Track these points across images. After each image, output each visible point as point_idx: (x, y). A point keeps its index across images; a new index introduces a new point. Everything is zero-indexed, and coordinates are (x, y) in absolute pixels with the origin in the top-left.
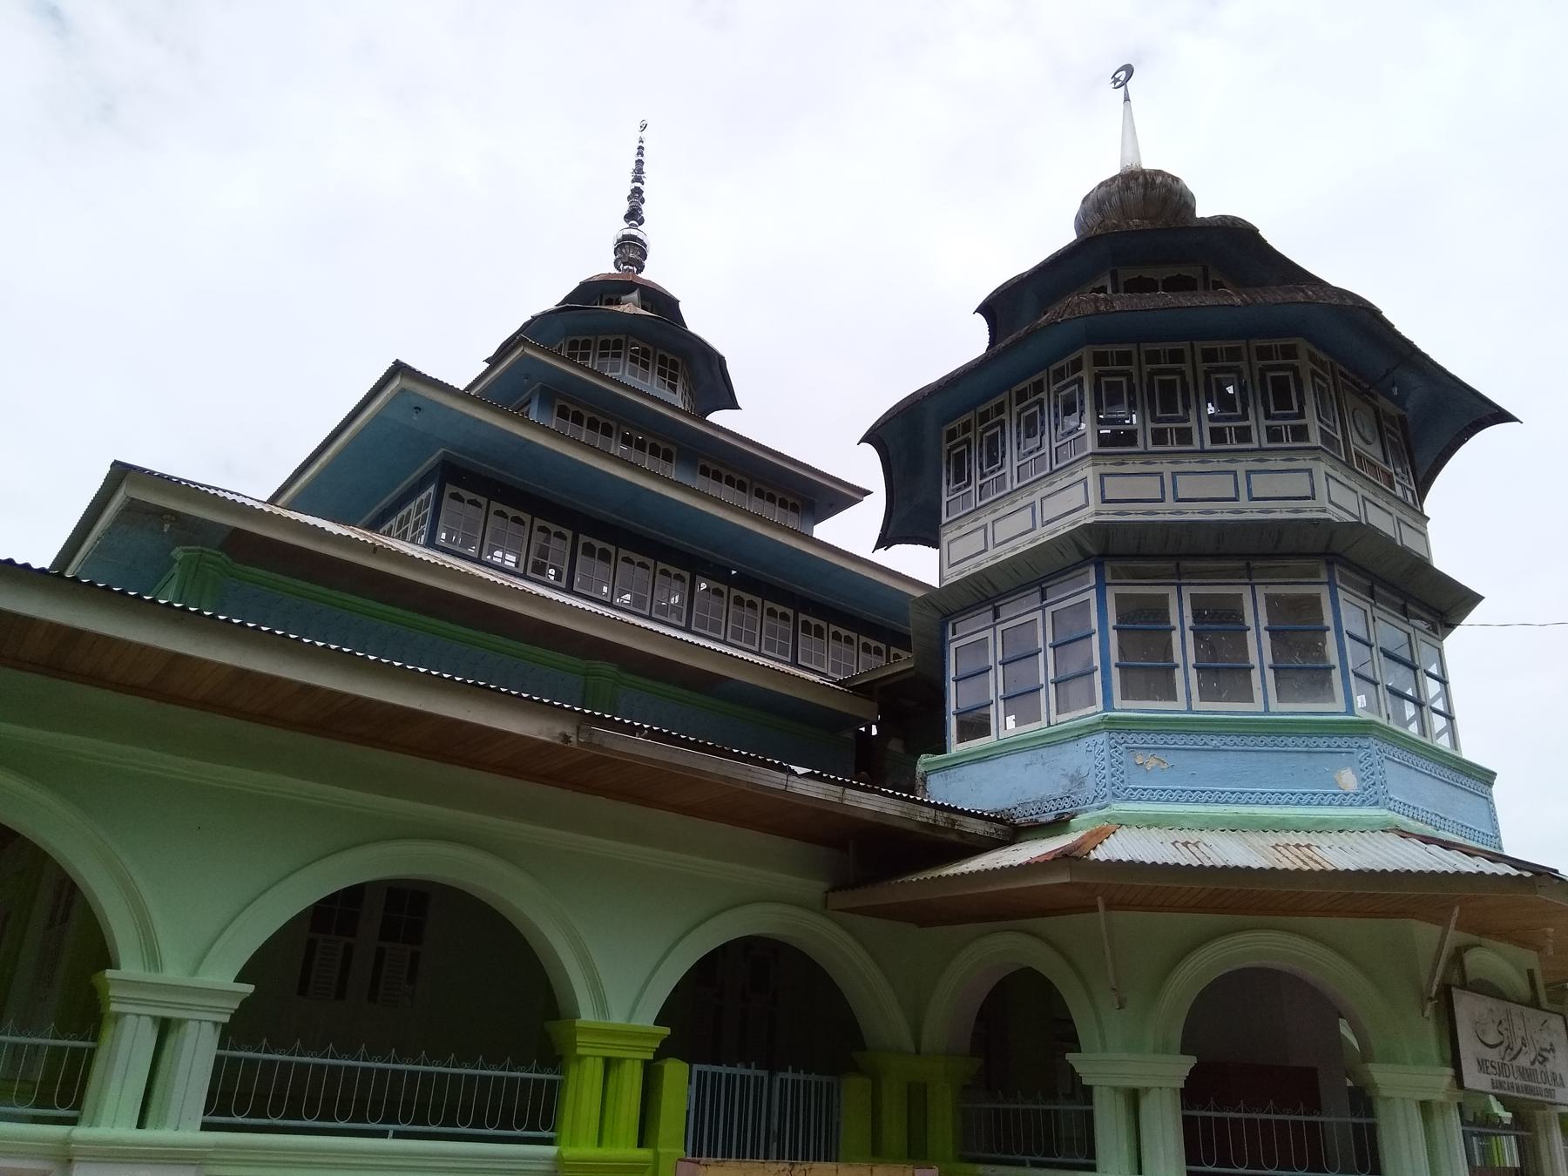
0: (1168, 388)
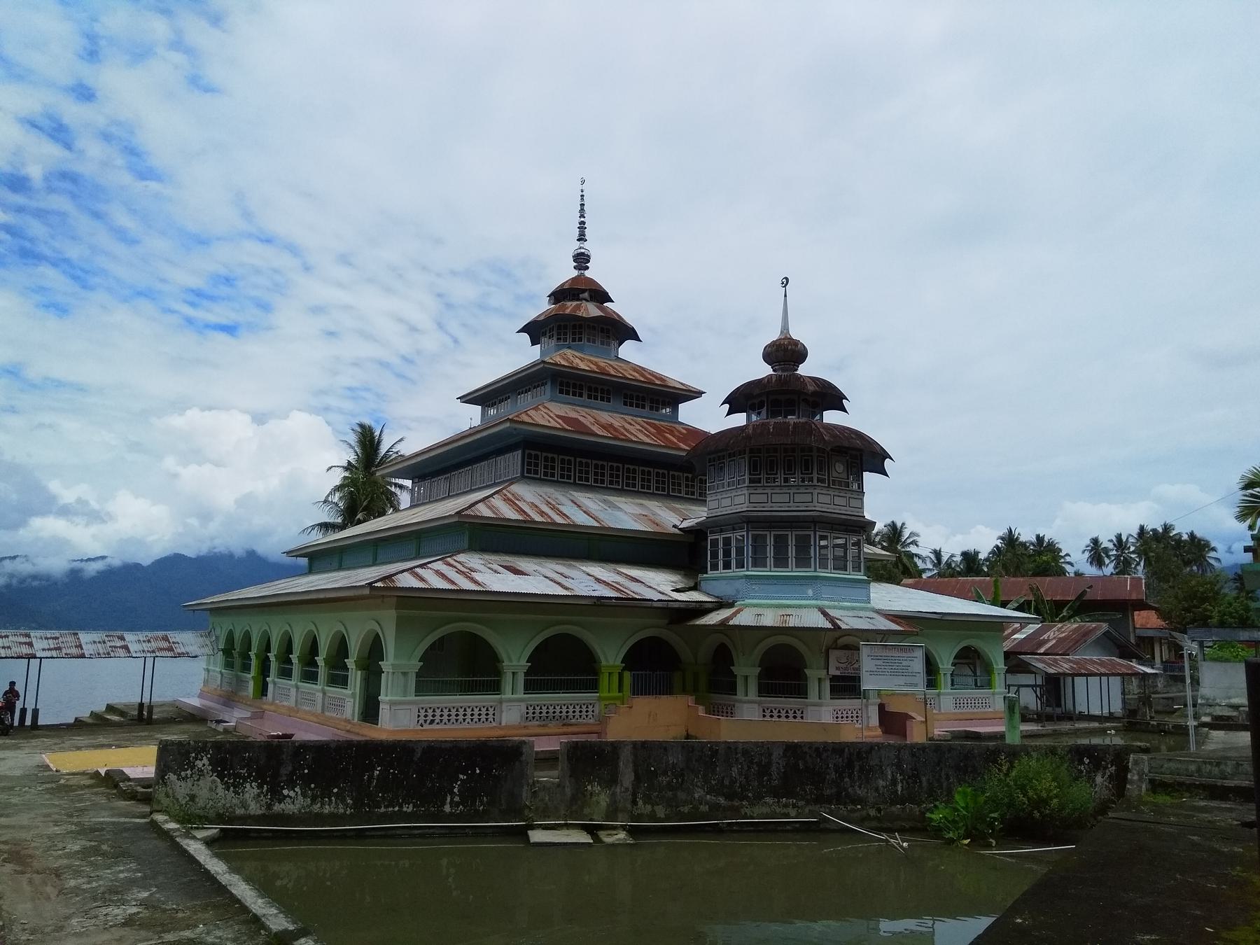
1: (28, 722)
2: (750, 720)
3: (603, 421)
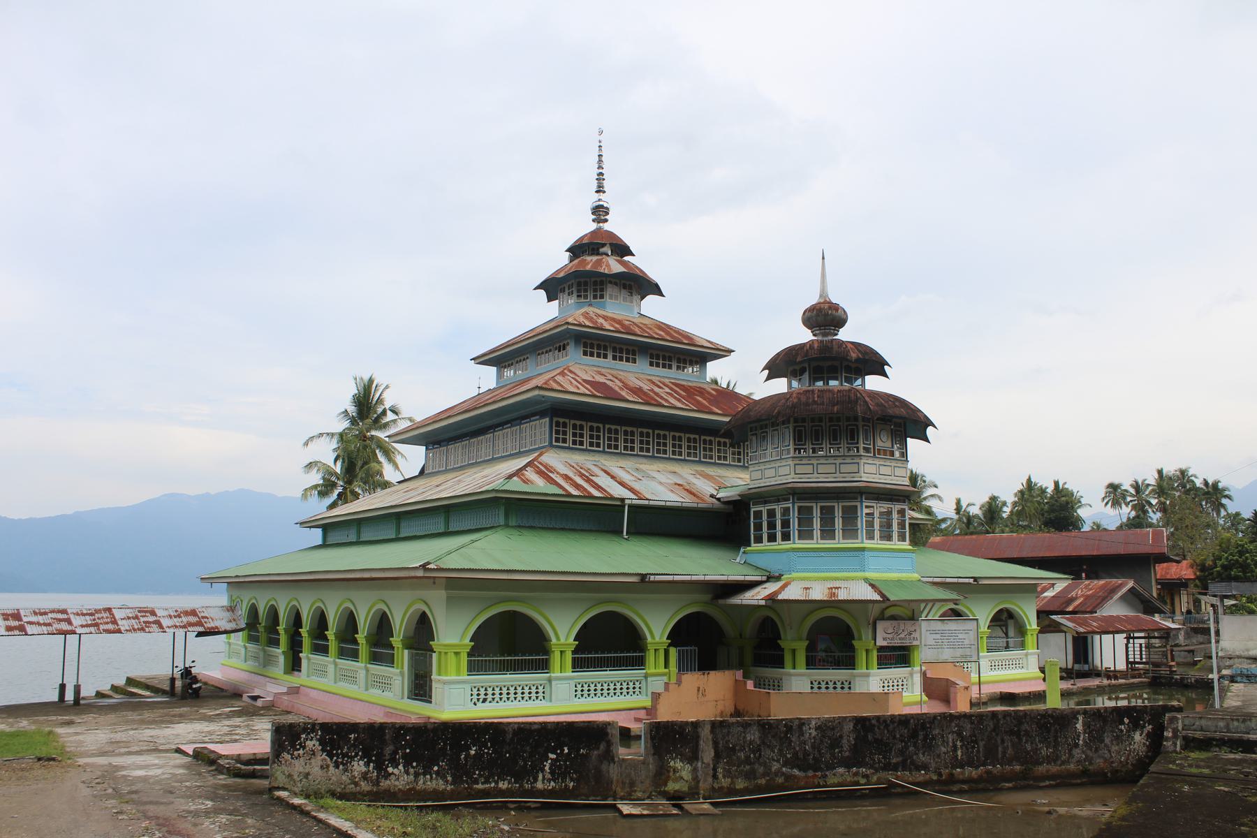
0: (817, 431)
1: (70, 696)
2: (800, 691)
3: (631, 384)
